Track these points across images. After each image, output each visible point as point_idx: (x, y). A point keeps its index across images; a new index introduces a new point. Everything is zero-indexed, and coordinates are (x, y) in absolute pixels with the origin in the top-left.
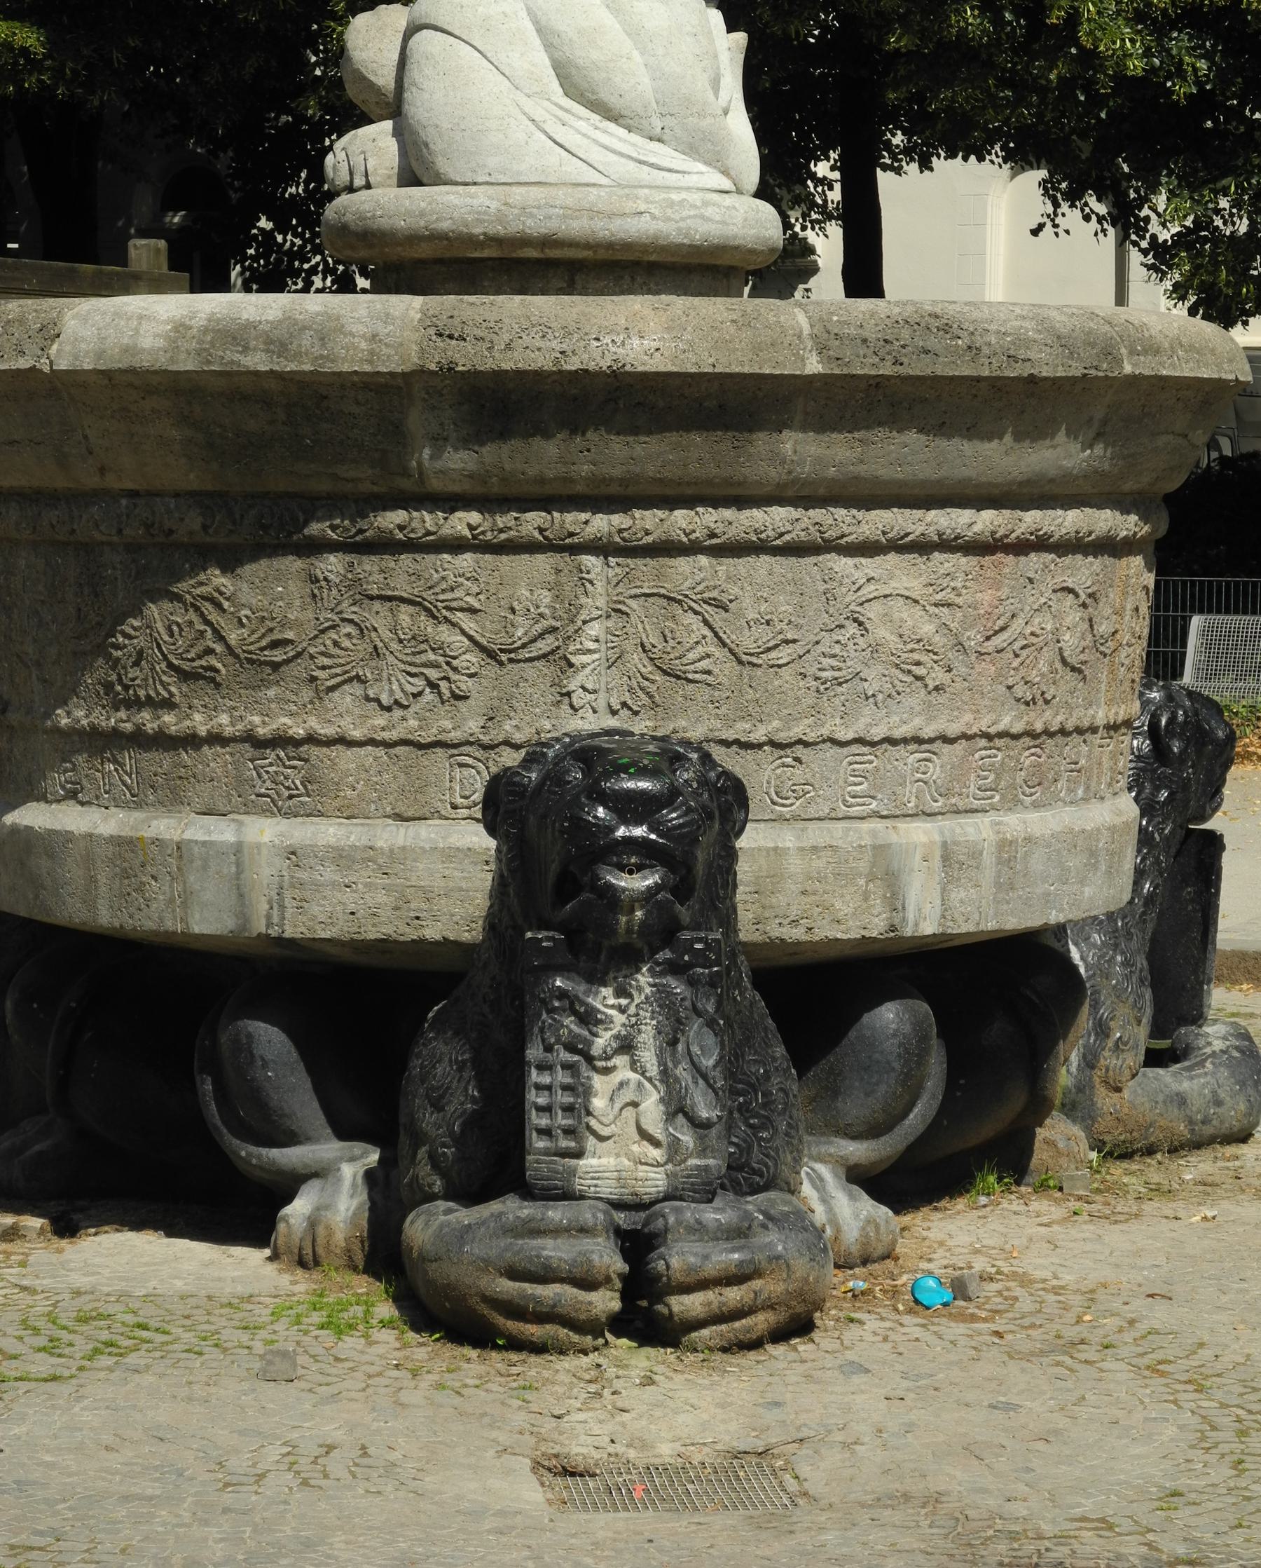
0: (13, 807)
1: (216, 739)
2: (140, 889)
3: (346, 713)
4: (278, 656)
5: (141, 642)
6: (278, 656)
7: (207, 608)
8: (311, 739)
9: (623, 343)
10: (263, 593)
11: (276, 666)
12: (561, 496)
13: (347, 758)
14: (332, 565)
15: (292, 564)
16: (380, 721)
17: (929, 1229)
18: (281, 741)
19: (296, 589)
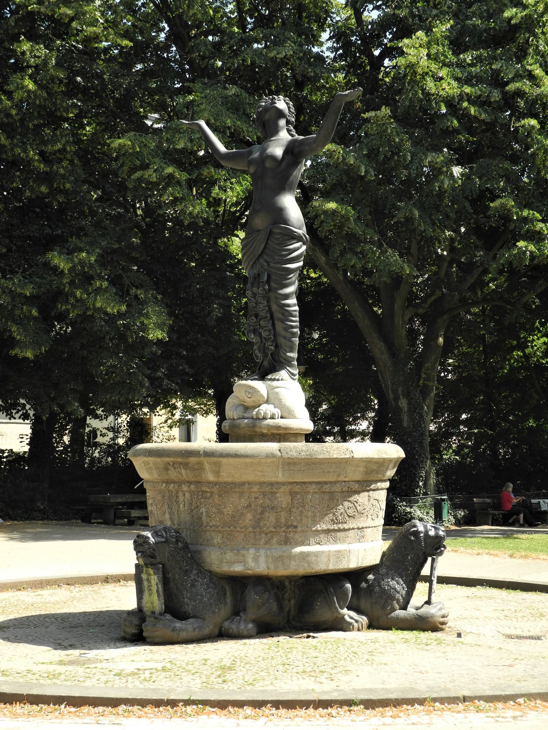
0: (293, 548)
1: (353, 529)
4: (363, 512)
13: (368, 530)
15: (366, 494)
19: (367, 498)
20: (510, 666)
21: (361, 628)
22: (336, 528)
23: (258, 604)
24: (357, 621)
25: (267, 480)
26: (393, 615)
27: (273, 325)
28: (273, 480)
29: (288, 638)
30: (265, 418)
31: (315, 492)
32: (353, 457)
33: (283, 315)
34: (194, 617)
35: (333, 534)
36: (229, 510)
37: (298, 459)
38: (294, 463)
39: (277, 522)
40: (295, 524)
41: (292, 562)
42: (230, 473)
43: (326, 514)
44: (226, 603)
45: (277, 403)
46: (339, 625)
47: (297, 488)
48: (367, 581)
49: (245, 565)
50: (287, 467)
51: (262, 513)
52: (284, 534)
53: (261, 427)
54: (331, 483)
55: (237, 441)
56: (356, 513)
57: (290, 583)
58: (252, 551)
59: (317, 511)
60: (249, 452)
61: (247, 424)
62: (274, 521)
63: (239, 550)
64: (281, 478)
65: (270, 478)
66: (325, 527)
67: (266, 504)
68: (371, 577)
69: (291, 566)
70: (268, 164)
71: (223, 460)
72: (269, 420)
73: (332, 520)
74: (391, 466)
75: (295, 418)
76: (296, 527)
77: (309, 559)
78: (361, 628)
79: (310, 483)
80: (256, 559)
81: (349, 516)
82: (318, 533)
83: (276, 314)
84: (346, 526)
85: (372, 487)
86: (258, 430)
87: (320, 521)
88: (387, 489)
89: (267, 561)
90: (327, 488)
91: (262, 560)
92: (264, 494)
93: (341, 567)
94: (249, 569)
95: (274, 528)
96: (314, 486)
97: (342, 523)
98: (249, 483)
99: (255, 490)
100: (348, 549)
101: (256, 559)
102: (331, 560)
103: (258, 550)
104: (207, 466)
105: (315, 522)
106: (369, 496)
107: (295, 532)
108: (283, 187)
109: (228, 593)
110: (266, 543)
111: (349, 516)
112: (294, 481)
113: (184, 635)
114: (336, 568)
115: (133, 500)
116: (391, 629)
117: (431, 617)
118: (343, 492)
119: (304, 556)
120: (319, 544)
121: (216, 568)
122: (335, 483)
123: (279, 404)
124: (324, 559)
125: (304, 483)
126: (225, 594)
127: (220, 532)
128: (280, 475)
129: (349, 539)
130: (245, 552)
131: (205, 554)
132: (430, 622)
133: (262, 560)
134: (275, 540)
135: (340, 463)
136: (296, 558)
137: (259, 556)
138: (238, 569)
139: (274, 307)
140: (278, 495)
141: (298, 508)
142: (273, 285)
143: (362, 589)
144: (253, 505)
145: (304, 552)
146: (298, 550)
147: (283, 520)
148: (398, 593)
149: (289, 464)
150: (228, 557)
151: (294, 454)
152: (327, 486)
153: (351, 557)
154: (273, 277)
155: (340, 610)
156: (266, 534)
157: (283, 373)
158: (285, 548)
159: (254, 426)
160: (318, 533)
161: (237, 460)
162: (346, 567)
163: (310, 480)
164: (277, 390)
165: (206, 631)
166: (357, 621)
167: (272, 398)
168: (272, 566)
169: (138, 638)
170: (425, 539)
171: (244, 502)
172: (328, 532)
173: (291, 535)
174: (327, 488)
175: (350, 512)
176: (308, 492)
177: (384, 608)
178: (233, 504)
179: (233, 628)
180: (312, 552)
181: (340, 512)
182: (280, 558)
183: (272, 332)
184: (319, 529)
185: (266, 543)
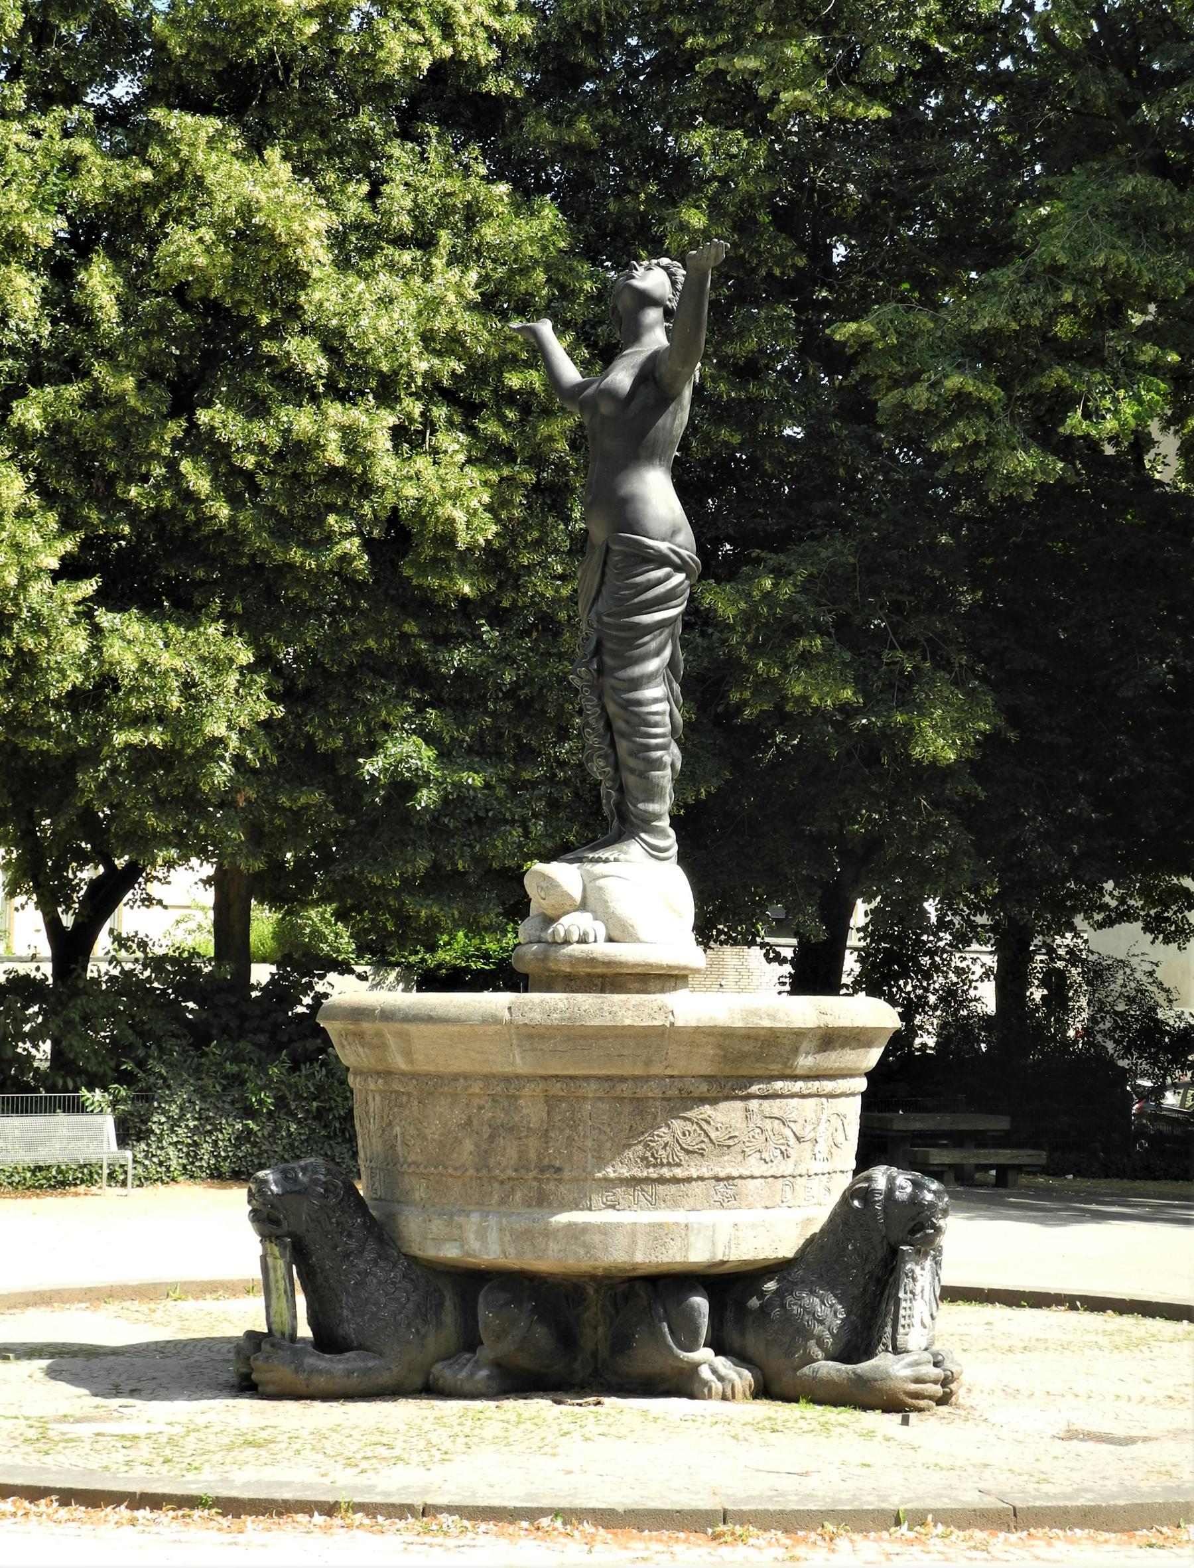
0: (555, 1214)
1: (701, 1178)
2: (663, 1245)
3: (754, 1166)
4: (731, 1142)
5: (667, 1139)
6: (731, 1142)
7: (703, 1124)
8: (741, 1177)
9: (347, 1255)
10: (726, 1115)
11: (729, 1147)
12: (18, 1358)
13: (751, 1183)
14: (754, 1104)
15: (739, 1104)
16: (764, 1167)
17: (122, 1166)
18: (730, 1178)
19: (741, 1114)
20: (801, 1475)
21: (729, 1393)
22: (655, 1176)
23: (505, 1331)
24: (721, 1379)
25: (497, 1069)
26: (806, 1370)
27: (613, 744)
28: (508, 1069)
29: (549, 1402)
30: (567, 942)
31: (600, 1098)
32: (672, 1024)
33: (627, 722)
34: (361, 1347)
35: (648, 1188)
36: (433, 1130)
37: (548, 1027)
38: (542, 1037)
39: (520, 1158)
40: (558, 1163)
41: (551, 1244)
42: (430, 1054)
43: (629, 1146)
44: (439, 1324)
45: (599, 909)
46: (683, 1384)
47: (557, 1089)
48: (761, 1295)
49: (462, 1246)
50: (527, 1045)
51: (491, 1138)
52: (535, 1183)
53: (557, 961)
54: (635, 1078)
55: (548, 989)
56: (707, 1146)
57: (597, 1291)
58: (475, 1218)
59: (603, 1138)
60: (453, 1012)
61: (534, 953)
62: (515, 1157)
63: (452, 1215)
64: (520, 1064)
65: (500, 1067)
66: (625, 1172)
67: (499, 1121)
68: (771, 1286)
69: (550, 1253)
70: (605, 408)
71: (411, 1028)
72: (575, 946)
73: (644, 1159)
74: (805, 1046)
75: (638, 940)
76: (559, 1170)
77: (587, 1238)
78: (729, 1393)
79: (587, 1078)
80: (482, 1234)
81: (688, 1152)
82: (609, 1184)
83: (622, 724)
84: (679, 1172)
85: (754, 1089)
86: (552, 965)
87: (613, 1159)
88: (863, 1094)
89: (501, 1239)
90: (625, 1089)
91: (493, 1236)
92: (494, 1099)
93: (666, 1260)
94: (469, 1255)
95: (516, 1170)
96: (594, 1085)
97: (669, 1164)
98: (466, 1077)
99: (477, 1090)
100: (683, 1221)
101: (482, 1234)
102: (640, 1242)
103: (485, 1215)
104: (391, 1041)
105: (601, 1162)
106: (747, 1110)
107: (560, 1181)
108: (638, 451)
109: (448, 1304)
110: (502, 1202)
111: (688, 1152)
112: (551, 1072)
113: (321, 1382)
114: (654, 1259)
115: (955, 1127)
116: (797, 1401)
117: (883, 1379)
118: (669, 1099)
119: (576, 1232)
120: (613, 1207)
121: (416, 1250)
122: (647, 1078)
123: (603, 913)
124: (621, 1240)
125: (572, 1078)
126: (440, 1305)
127: (423, 1176)
128: (518, 1061)
129: (691, 1200)
130: (460, 1219)
131: (401, 1220)
132: (880, 1390)
133: (493, 1236)
134: (518, 1196)
135: (645, 1037)
136: (560, 1234)
137: (486, 1229)
138: (450, 1252)
139: (612, 708)
140: (521, 1102)
141: (562, 1131)
142: (608, 661)
143: (751, 1311)
144: (475, 1122)
145: (576, 1224)
146: (563, 1218)
147: (532, 1155)
148: (821, 1322)
149: (530, 1037)
150: (435, 1230)
151: (538, 1017)
152: (624, 1086)
153: (692, 1239)
154: (608, 645)
155: (683, 1355)
156: (502, 1183)
157: (633, 850)
158: (537, 1213)
159: (545, 958)
160: (609, 1184)
161: (431, 1027)
162: (679, 1259)
163: (586, 1072)
164: (601, 882)
165: (385, 1378)
166: (721, 1379)
167: (591, 901)
168: (511, 1251)
169: (247, 1386)
170: (885, 1207)
171: (457, 1116)
172: (633, 1182)
173: (552, 1186)
174: (625, 1089)
175: (690, 1142)
176: (585, 1098)
177: (789, 1354)
178: (443, 1117)
179: (444, 1373)
180: (594, 1225)
181: (661, 1142)
182: (526, 1235)
183: (612, 759)
184: (612, 1175)
185: (502, 1202)
